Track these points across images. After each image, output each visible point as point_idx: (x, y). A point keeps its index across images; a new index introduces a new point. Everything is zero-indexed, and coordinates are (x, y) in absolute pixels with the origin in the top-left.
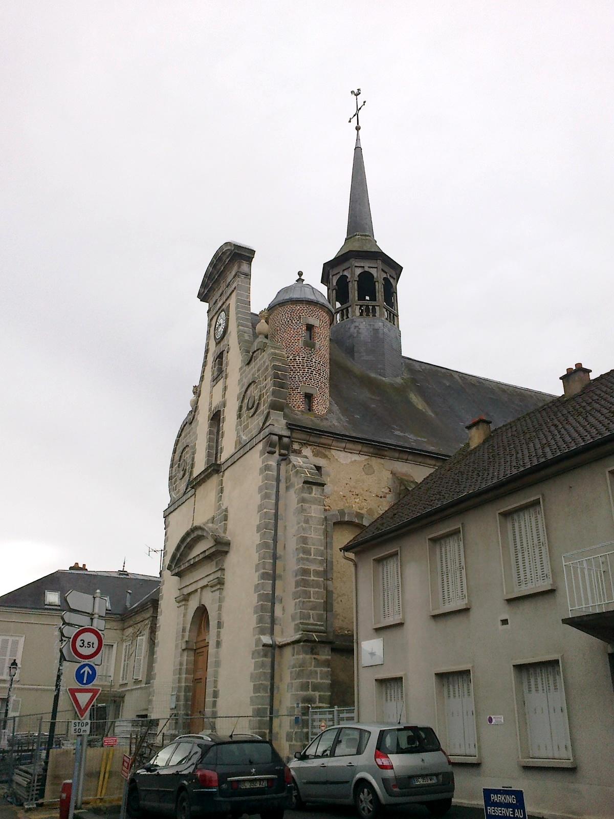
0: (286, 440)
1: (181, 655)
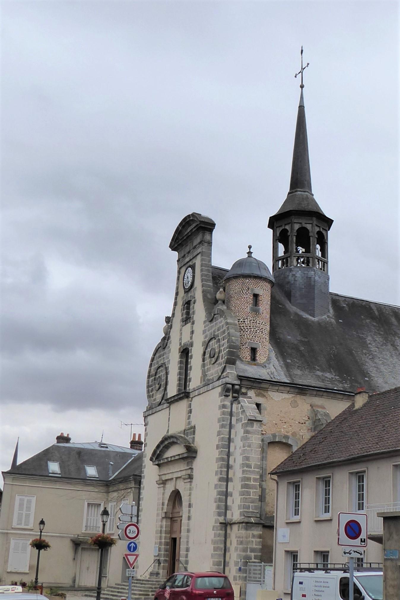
0: (237, 387)
1: (162, 521)
